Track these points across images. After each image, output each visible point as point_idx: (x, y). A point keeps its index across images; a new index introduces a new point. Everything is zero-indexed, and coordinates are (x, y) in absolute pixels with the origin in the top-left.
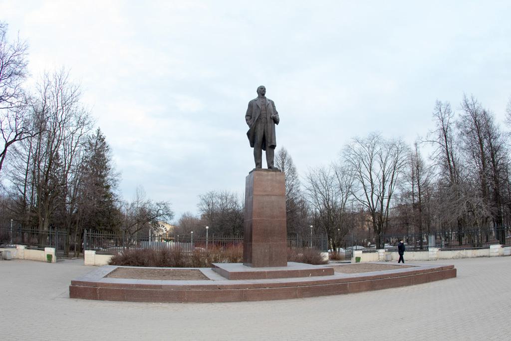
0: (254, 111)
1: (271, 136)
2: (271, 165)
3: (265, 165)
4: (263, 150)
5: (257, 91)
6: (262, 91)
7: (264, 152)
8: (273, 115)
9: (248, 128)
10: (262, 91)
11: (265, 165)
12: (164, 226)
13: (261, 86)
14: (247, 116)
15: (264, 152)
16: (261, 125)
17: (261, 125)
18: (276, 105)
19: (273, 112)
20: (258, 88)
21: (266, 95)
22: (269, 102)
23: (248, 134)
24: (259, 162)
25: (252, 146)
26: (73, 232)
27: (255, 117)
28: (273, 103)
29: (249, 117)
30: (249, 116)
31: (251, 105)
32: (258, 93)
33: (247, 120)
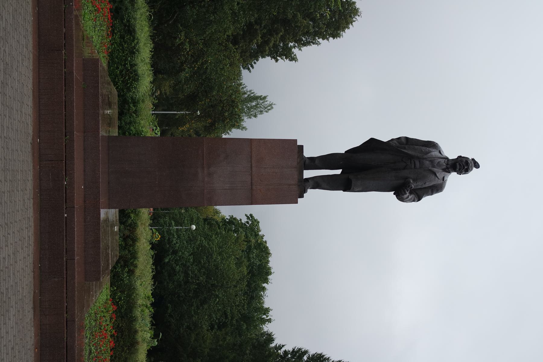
2: (311, 183)
3: (308, 174)
5: (460, 157)
6: (463, 165)
10: (463, 165)
11: (308, 174)
14: (407, 138)
18: (436, 196)
19: (420, 184)
21: (454, 175)
25: (346, 152)
26: (130, 123)
27: (405, 148)
29: (403, 140)
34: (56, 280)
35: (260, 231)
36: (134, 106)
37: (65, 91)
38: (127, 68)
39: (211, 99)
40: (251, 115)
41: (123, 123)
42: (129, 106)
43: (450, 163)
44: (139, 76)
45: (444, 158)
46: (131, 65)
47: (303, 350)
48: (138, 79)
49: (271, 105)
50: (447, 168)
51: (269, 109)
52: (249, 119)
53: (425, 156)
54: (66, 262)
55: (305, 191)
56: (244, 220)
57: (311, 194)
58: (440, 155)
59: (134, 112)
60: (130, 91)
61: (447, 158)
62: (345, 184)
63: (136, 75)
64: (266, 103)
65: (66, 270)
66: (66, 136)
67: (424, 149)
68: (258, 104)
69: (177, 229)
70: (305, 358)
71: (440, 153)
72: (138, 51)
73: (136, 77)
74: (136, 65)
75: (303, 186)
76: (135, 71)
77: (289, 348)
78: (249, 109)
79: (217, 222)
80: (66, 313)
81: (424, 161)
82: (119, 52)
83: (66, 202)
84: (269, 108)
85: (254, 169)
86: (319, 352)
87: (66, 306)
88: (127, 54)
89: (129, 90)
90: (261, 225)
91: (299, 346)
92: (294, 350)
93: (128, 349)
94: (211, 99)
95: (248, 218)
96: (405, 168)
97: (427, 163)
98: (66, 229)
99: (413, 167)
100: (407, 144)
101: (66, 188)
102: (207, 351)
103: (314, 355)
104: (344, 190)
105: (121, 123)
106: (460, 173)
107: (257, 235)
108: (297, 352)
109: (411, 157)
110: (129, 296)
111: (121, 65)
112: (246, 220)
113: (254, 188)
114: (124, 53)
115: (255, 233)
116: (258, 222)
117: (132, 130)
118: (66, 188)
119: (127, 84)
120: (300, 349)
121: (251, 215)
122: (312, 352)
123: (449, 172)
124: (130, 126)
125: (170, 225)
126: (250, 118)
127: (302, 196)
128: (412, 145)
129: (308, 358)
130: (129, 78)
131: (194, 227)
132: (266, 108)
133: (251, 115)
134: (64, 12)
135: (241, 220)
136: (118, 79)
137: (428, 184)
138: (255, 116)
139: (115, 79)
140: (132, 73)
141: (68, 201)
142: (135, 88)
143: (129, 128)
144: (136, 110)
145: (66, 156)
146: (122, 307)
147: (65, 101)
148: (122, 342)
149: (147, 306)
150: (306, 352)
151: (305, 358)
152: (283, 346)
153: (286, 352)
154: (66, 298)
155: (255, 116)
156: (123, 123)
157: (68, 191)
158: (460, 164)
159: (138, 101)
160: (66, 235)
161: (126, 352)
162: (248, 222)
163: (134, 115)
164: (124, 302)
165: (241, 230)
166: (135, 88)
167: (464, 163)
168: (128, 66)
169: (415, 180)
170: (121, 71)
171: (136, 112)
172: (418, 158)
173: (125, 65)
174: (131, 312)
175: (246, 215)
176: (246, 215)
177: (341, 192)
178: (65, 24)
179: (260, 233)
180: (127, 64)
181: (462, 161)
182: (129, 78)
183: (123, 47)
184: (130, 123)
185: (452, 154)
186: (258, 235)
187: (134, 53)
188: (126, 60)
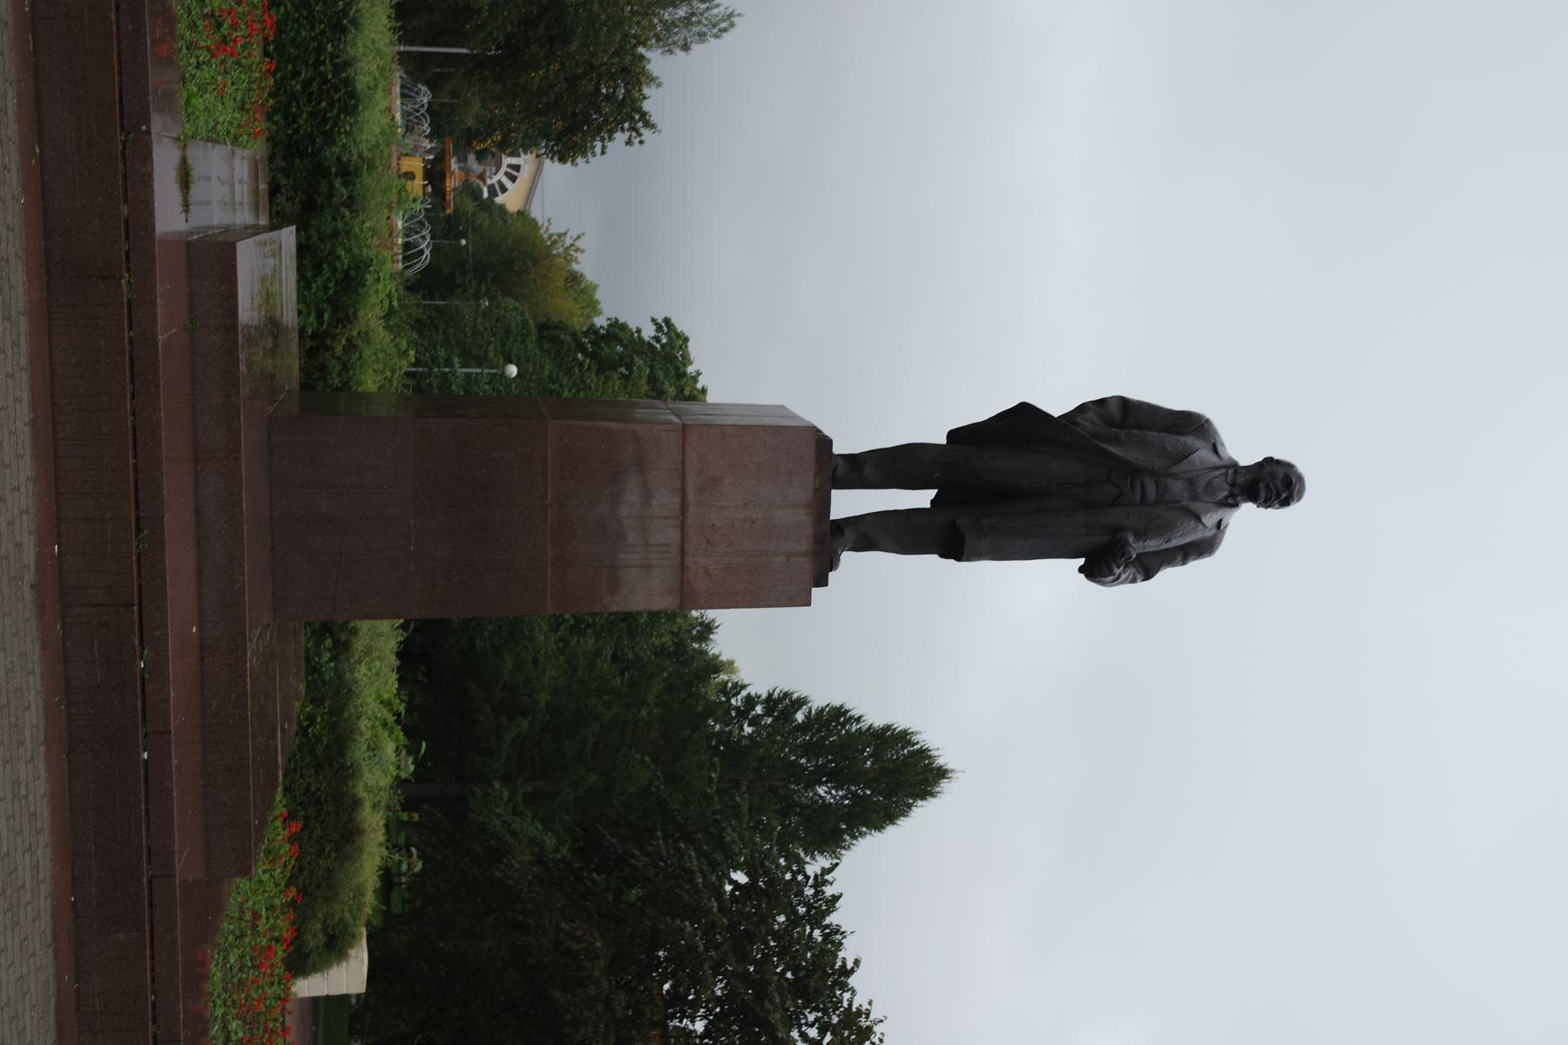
0: (1152, 435)
1: (256, 174)
2: (849, 535)
3: (848, 503)
4: (932, 493)
5: (1269, 460)
6: (1274, 484)
7: (922, 498)
8: (1136, 547)
9: (1057, 404)
10: (1274, 484)
11: (848, 503)
12: (513, 179)
13: (1300, 478)
14: (1124, 402)
15: (922, 498)
16: (1099, 486)
17: (1099, 486)
18: (1196, 566)
19: (1153, 545)
20: (1290, 466)
21: (1248, 509)
22: (1210, 520)
23: (1025, 412)
24: (868, 470)
25: (952, 435)
26: (335, 234)
27: (1116, 441)
28: (1204, 547)
29: (1115, 410)
30: (1120, 418)
31: (1192, 425)
32: (1260, 465)
33: (1101, 403)
34: (122, 936)
35: (690, 363)
36: (346, 184)
37: (133, 396)
38: (323, 76)
39: (563, 64)
40: (674, 43)
41: (315, 237)
42: (332, 187)
43: (1241, 479)
44: (358, 100)
45: (1227, 467)
46: (335, 66)
47: (795, 696)
48: (356, 107)
49: (731, 15)
50: (1232, 495)
51: (725, 30)
52: (668, 57)
53: (1174, 470)
54: (150, 882)
55: (832, 564)
56: (648, 332)
57: (851, 562)
58: (1214, 459)
59: (345, 204)
60: (334, 142)
61: (1234, 465)
62: (944, 533)
63: (352, 95)
64: (715, 11)
65: (151, 905)
66: (139, 530)
67: (1170, 440)
68: (693, 14)
69: (468, 375)
70: (800, 717)
71: (1216, 451)
72: (355, 23)
73: (350, 834)
74: (348, 64)
75: (832, 541)
76: (348, 82)
77: (759, 686)
78: (669, 26)
79: (574, 335)
80: (154, 1021)
81: (1170, 481)
82: (300, 26)
83: (144, 720)
84: (724, 25)
85: (692, 510)
86: (837, 703)
87: (154, 1003)
88: (323, 32)
89: (330, 138)
90: (692, 348)
91: (785, 686)
92: (770, 695)
93: (337, 849)
94: (563, 64)
95: (659, 328)
96: (1114, 504)
97: (1177, 487)
98: (147, 795)
99: (1138, 498)
100: (1120, 425)
101: (143, 680)
102: (544, 698)
103: (823, 710)
104: (944, 555)
105: (309, 238)
106: (1267, 503)
107: (681, 375)
108: (780, 700)
109: (1133, 472)
110: (337, 711)
111: (306, 64)
112: (653, 334)
113: (689, 560)
114: (313, 27)
115: (677, 368)
116: (686, 340)
117: (339, 258)
118: (143, 680)
119: (325, 121)
120: (786, 695)
121: (667, 321)
122: (818, 701)
123: (1236, 505)
124: (333, 245)
125: (449, 363)
126: (671, 52)
127: (822, 582)
128: (1139, 428)
129: (808, 717)
130: (331, 104)
131: (513, 370)
132: (714, 26)
133: (674, 43)
134: (124, 156)
135: (639, 331)
136: (298, 106)
137: (1176, 542)
138: (686, 47)
139: (290, 103)
140: (337, 90)
141: (149, 715)
142: (348, 133)
143: (332, 252)
144: (350, 197)
145: (140, 586)
146: (318, 738)
147: (134, 427)
148: (318, 832)
149: (385, 724)
150: (801, 702)
151: (800, 717)
152: (744, 687)
153: (750, 701)
154: (153, 980)
155: (686, 47)
156: (315, 237)
157: (149, 687)
158: (1268, 486)
159: (357, 169)
160: (147, 812)
161: (329, 855)
162: (657, 339)
163: (347, 213)
164: (323, 728)
165: (639, 361)
166: (348, 133)
167: (1279, 483)
168: (326, 68)
169: (1141, 535)
170: (307, 84)
171: (350, 202)
172: (1154, 473)
173: (318, 63)
174: (342, 754)
175: (653, 320)
176: (653, 320)
177: (933, 559)
178: (126, 191)
179: (691, 369)
180: (323, 63)
181: (1273, 476)
182: (331, 104)
183: (311, 11)
184: (335, 234)
185: (1243, 449)
186: (684, 374)
187: (343, 30)
188: (320, 50)
